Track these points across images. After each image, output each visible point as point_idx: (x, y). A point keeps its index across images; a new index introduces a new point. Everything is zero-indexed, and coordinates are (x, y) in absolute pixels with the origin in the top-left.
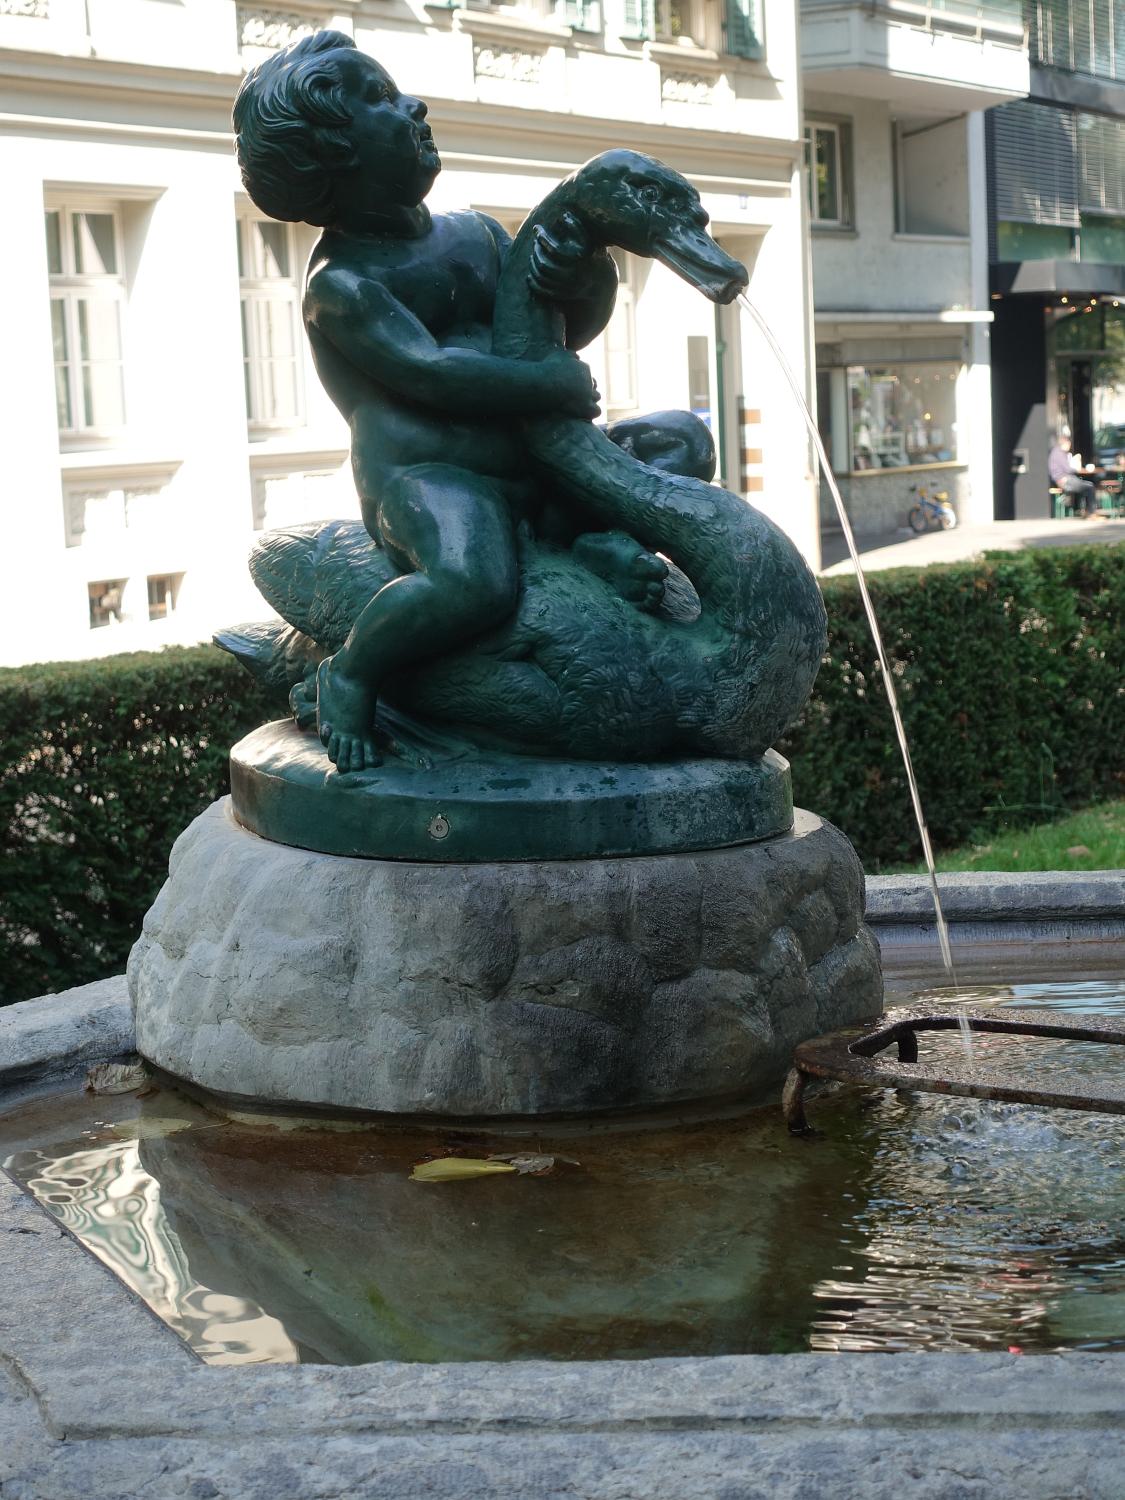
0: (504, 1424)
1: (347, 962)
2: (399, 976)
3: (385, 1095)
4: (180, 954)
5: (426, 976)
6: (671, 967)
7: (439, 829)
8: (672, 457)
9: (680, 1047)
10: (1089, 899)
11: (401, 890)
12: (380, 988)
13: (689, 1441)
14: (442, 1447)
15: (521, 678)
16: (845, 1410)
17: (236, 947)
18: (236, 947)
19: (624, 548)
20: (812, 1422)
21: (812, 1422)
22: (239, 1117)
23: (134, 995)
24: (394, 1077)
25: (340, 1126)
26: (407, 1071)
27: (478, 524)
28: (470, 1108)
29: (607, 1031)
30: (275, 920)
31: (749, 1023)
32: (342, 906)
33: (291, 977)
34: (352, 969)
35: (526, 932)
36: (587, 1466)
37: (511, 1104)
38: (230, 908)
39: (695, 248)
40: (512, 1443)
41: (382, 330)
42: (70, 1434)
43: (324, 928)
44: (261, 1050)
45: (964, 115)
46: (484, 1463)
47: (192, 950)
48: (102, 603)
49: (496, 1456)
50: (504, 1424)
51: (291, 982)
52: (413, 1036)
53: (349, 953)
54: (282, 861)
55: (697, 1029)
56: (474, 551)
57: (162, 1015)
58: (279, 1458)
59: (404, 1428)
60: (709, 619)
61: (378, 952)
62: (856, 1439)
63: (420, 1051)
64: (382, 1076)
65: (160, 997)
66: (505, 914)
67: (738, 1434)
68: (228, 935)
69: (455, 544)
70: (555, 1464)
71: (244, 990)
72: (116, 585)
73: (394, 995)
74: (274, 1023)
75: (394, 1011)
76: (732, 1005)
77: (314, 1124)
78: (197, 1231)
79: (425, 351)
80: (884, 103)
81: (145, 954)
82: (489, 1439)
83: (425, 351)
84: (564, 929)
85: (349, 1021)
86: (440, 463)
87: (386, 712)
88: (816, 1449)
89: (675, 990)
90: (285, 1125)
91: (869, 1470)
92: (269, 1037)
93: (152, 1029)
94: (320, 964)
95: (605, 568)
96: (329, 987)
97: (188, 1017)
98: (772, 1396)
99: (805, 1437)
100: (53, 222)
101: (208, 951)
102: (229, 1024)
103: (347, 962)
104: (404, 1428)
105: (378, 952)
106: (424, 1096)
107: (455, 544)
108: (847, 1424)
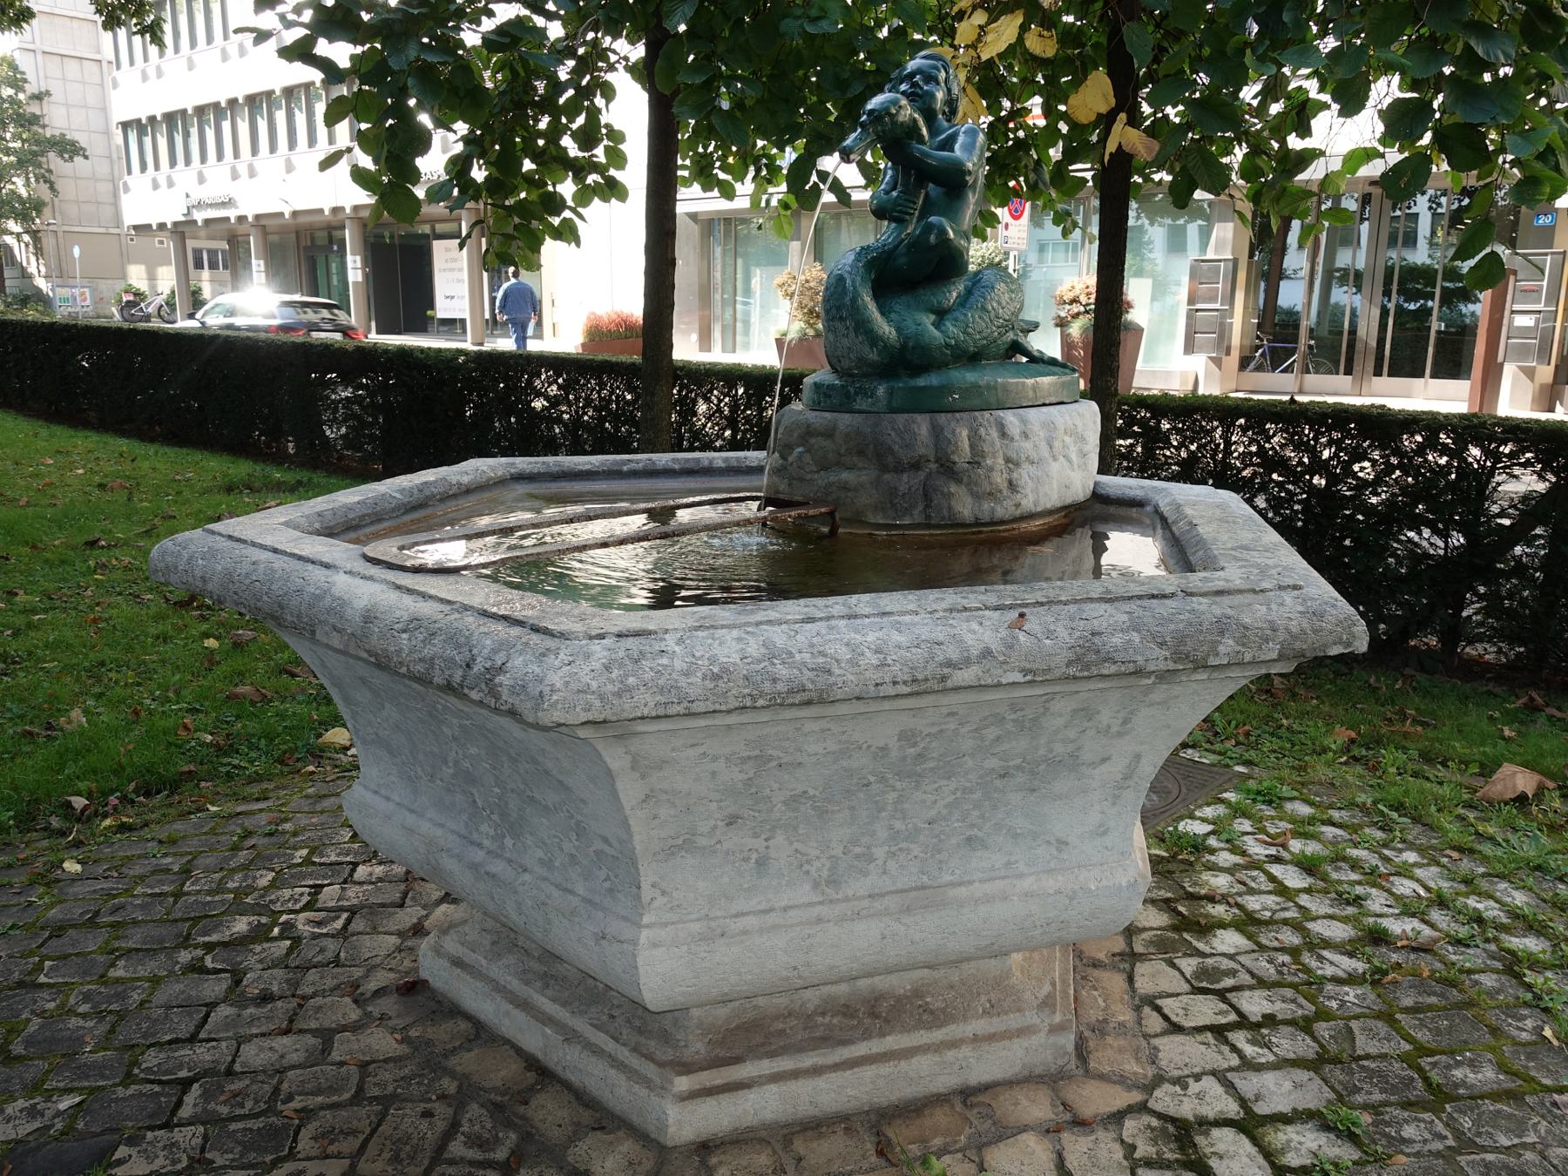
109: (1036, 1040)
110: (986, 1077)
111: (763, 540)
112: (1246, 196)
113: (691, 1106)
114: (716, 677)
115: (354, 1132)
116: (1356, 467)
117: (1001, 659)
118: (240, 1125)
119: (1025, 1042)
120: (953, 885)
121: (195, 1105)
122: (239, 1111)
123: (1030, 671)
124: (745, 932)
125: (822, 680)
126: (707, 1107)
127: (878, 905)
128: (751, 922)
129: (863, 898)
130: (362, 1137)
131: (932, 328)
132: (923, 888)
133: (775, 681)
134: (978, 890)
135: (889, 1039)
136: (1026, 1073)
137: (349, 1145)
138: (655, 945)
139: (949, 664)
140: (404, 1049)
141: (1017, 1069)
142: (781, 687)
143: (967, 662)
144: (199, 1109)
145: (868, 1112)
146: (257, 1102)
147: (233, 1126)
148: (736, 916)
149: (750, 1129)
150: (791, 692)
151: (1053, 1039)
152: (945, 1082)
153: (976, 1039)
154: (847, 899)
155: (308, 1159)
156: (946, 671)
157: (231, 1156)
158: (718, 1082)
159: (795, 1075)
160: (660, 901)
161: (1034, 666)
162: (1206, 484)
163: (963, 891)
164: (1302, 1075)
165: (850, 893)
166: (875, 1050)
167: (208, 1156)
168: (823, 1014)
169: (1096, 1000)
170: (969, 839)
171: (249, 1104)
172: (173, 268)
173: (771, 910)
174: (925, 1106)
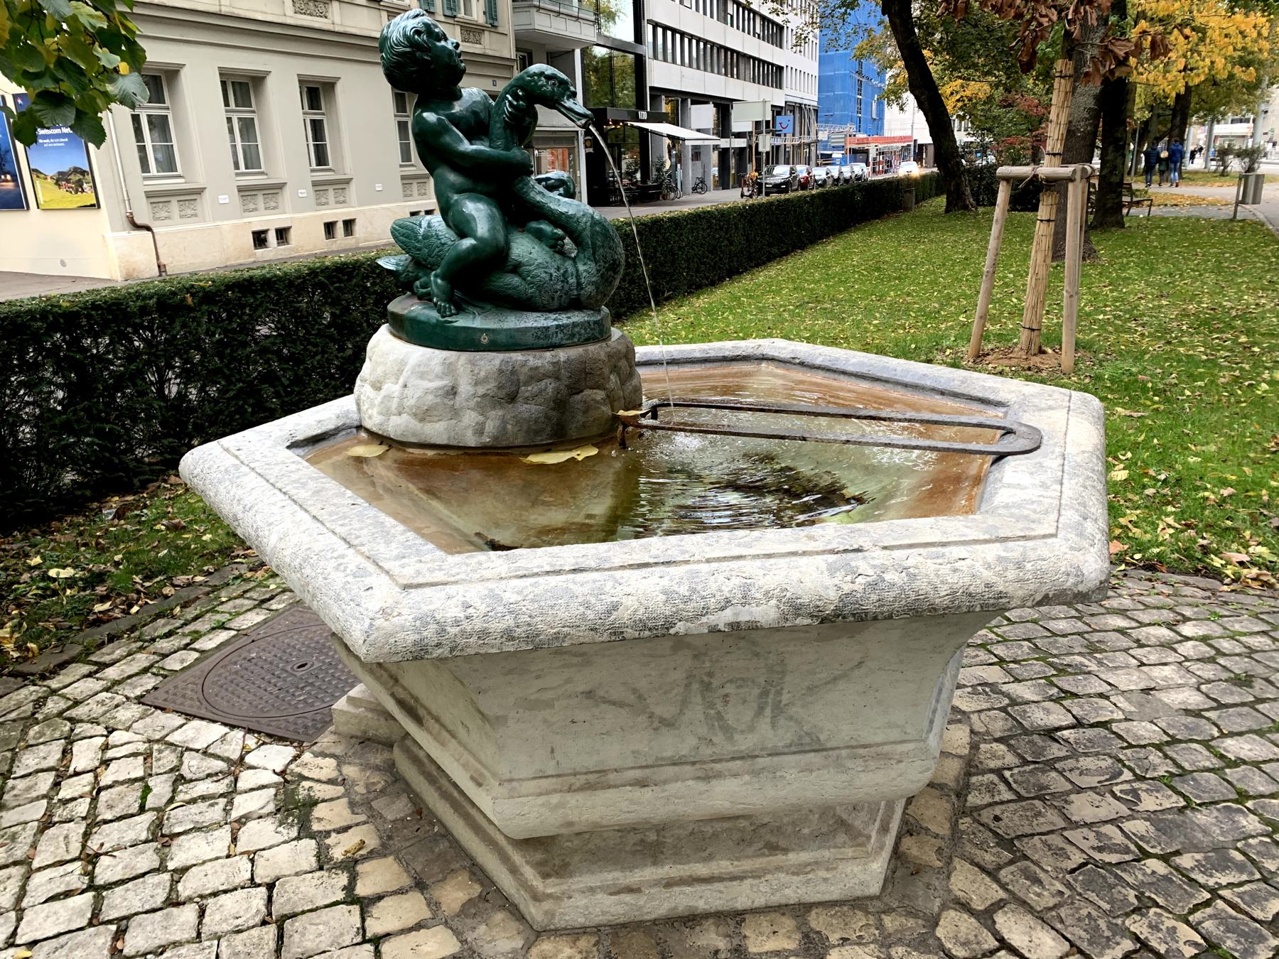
0: (574, 571)
1: (452, 392)
2: (474, 395)
3: (471, 440)
4: (379, 389)
5: (484, 396)
6: (575, 389)
7: (485, 339)
8: (561, 190)
9: (580, 418)
10: (698, 355)
11: (472, 363)
12: (467, 400)
13: (644, 571)
14: (554, 580)
15: (515, 280)
16: (697, 558)
17: (405, 386)
18: (405, 386)
19: (546, 227)
20: (687, 562)
21: (687, 562)
22: (411, 450)
23: (358, 405)
24: (474, 434)
25: (452, 453)
26: (480, 431)
27: (491, 218)
28: (504, 444)
29: (554, 413)
30: (422, 376)
31: (604, 408)
32: (449, 369)
33: (430, 397)
34: (455, 394)
35: (522, 378)
36: (610, 584)
37: (518, 442)
38: (401, 371)
39: (573, 106)
40: (579, 577)
41: (447, 139)
42: (406, 587)
43: (441, 378)
44: (419, 425)
45: (573, 51)
46: (571, 586)
47: (385, 387)
48: (260, 239)
49: (575, 583)
50: (574, 571)
51: (430, 398)
52: (481, 418)
53: (453, 388)
54: (417, 353)
55: (586, 412)
56: (492, 229)
57: (374, 412)
58: (492, 590)
59: (537, 574)
60: (582, 256)
61: (465, 388)
62: (704, 567)
63: (483, 424)
64: (469, 433)
65: (372, 405)
66: (513, 372)
67: (662, 568)
68: (401, 381)
69: (482, 228)
70: (598, 584)
71: (412, 402)
72: (265, 232)
73: (472, 403)
74: (424, 415)
75: (472, 409)
76: (598, 402)
77: (442, 452)
78: (373, 484)
79: (467, 146)
80: (544, 45)
81: (362, 385)
82: (571, 576)
83: (467, 146)
84: (536, 376)
85: (455, 413)
86: (472, 191)
87: (458, 294)
88: (691, 572)
89: (578, 397)
90: (430, 453)
91: (712, 578)
92: (422, 420)
93: (370, 417)
94: (440, 392)
95: (539, 236)
96: (446, 401)
97: (387, 413)
98: (670, 552)
99: (687, 567)
100: (224, 84)
101: (391, 388)
102: (405, 416)
103: (452, 392)
104: (537, 574)
105: (465, 388)
106: (486, 440)
107: (482, 228)
108: (699, 562)
111: (500, 413)
115: (1044, 843)
116: (21, 436)
118: (1102, 904)
121: (1118, 944)
122: (1094, 913)
130: (1043, 838)
131: (598, 213)
137: (1055, 840)
140: (957, 862)
144: (1118, 938)
146: (1079, 909)
147: (1106, 907)
155: (1083, 851)
157: (1123, 891)
162: (193, 447)
164: (257, 610)
167: (1136, 902)
171: (1084, 912)
172: (648, 85)
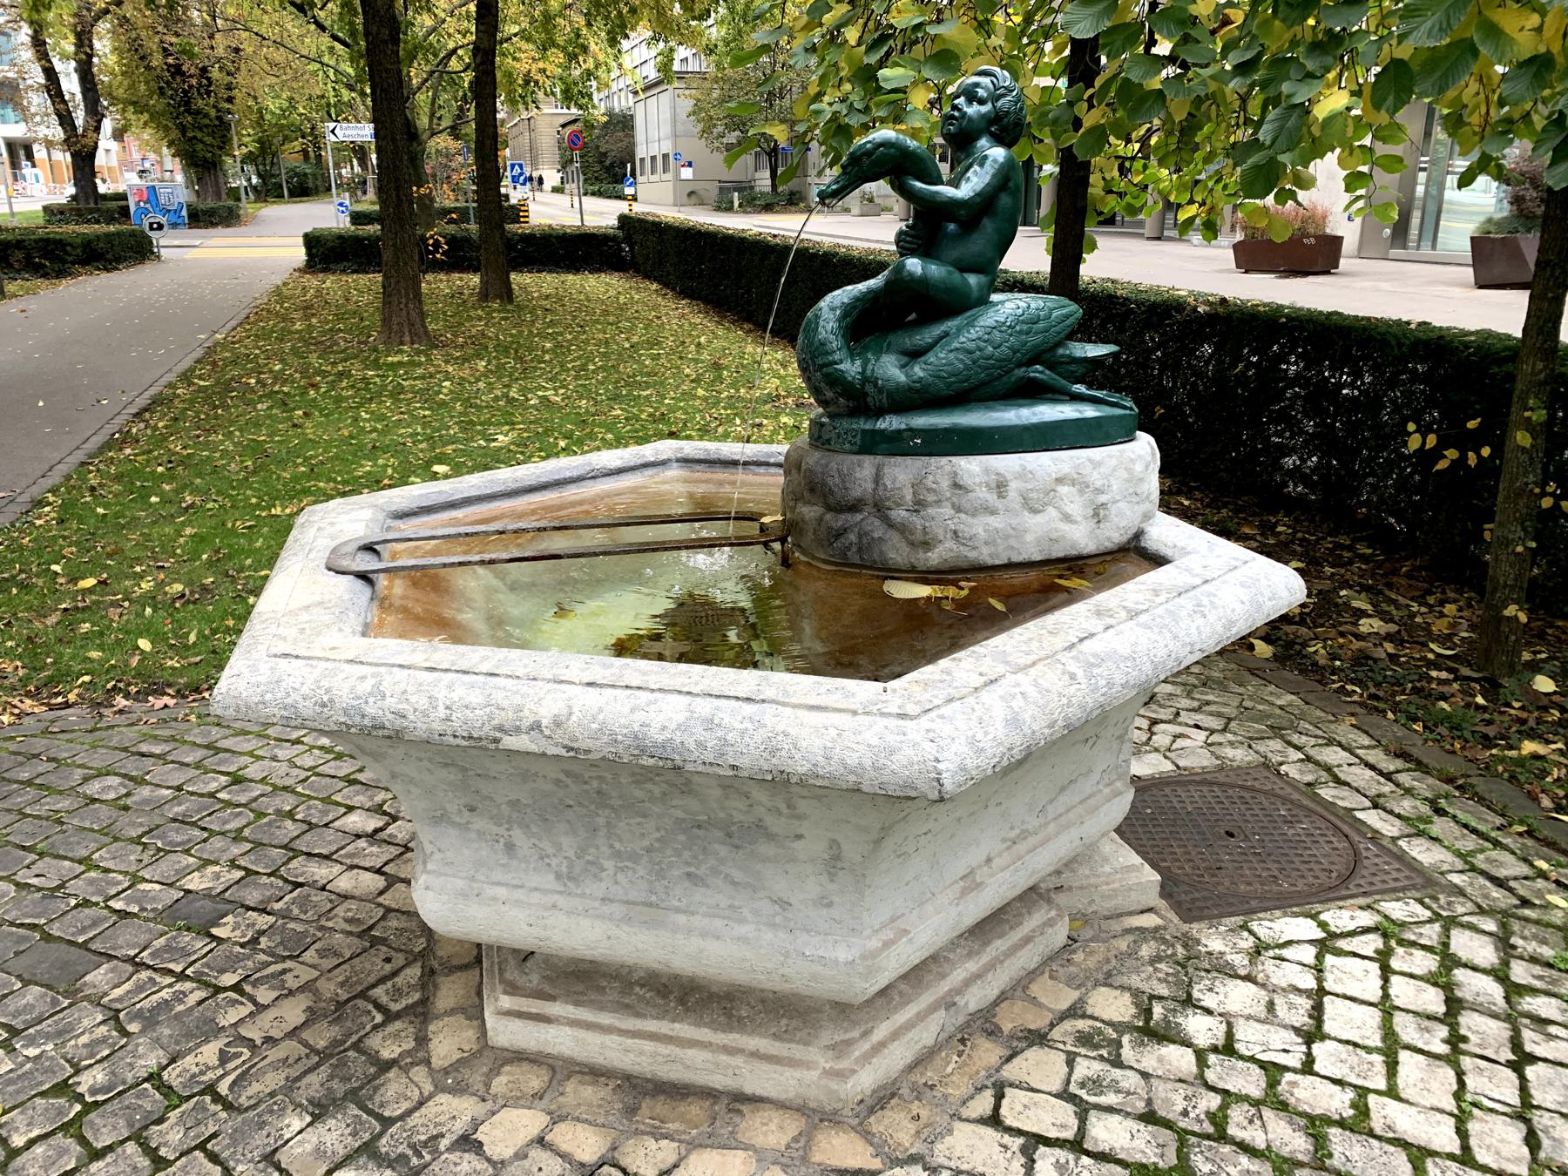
109: (813, 1075)
110: (759, 1092)
112: (1442, 90)
113: (505, 1021)
114: (324, 705)
117: (547, 732)
119: (797, 1074)
120: (678, 910)
123: (572, 749)
124: (494, 899)
125: (399, 723)
126: (517, 1025)
127: (606, 909)
128: (502, 892)
129: (596, 899)
132: (650, 905)
133: (363, 716)
134: (697, 921)
135: (677, 1026)
136: (800, 1101)
138: (427, 888)
139: (500, 729)
141: (791, 1095)
142: (366, 722)
143: (518, 730)
145: (648, 1080)
148: (493, 884)
149: (548, 1056)
150: (374, 727)
151: (824, 1082)
152: (718, 1081)
153: (755, 1055)
154: (583, 895)
156: (498, 735)
158: (534, 1010)
159: (589, 1026)
160: (437, 856)
161: (575, 745)
163: (682, 919)
165: (588, 892)
166: (664, 1031)
168: (642, 986)
169: (948, 1063)
170: (689, 875)
173: (521, 887)
174: (695, 1094)
